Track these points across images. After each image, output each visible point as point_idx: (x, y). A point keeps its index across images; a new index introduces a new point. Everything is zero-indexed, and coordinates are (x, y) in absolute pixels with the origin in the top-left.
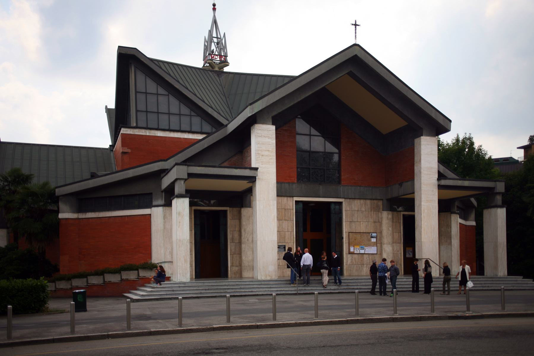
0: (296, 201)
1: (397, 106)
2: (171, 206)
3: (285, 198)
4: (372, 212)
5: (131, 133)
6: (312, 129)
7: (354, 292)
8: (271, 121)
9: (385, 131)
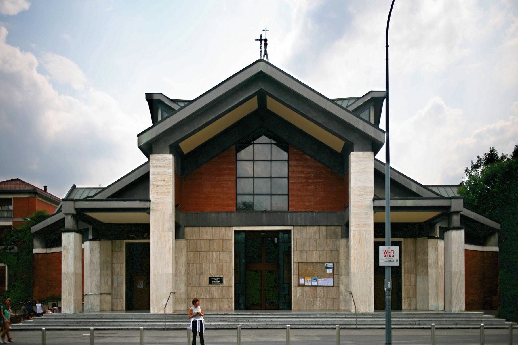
0: (235, 231)
3: (224, 228)
4: (328, 240)
7: (139, 329)
8: (168, 150)
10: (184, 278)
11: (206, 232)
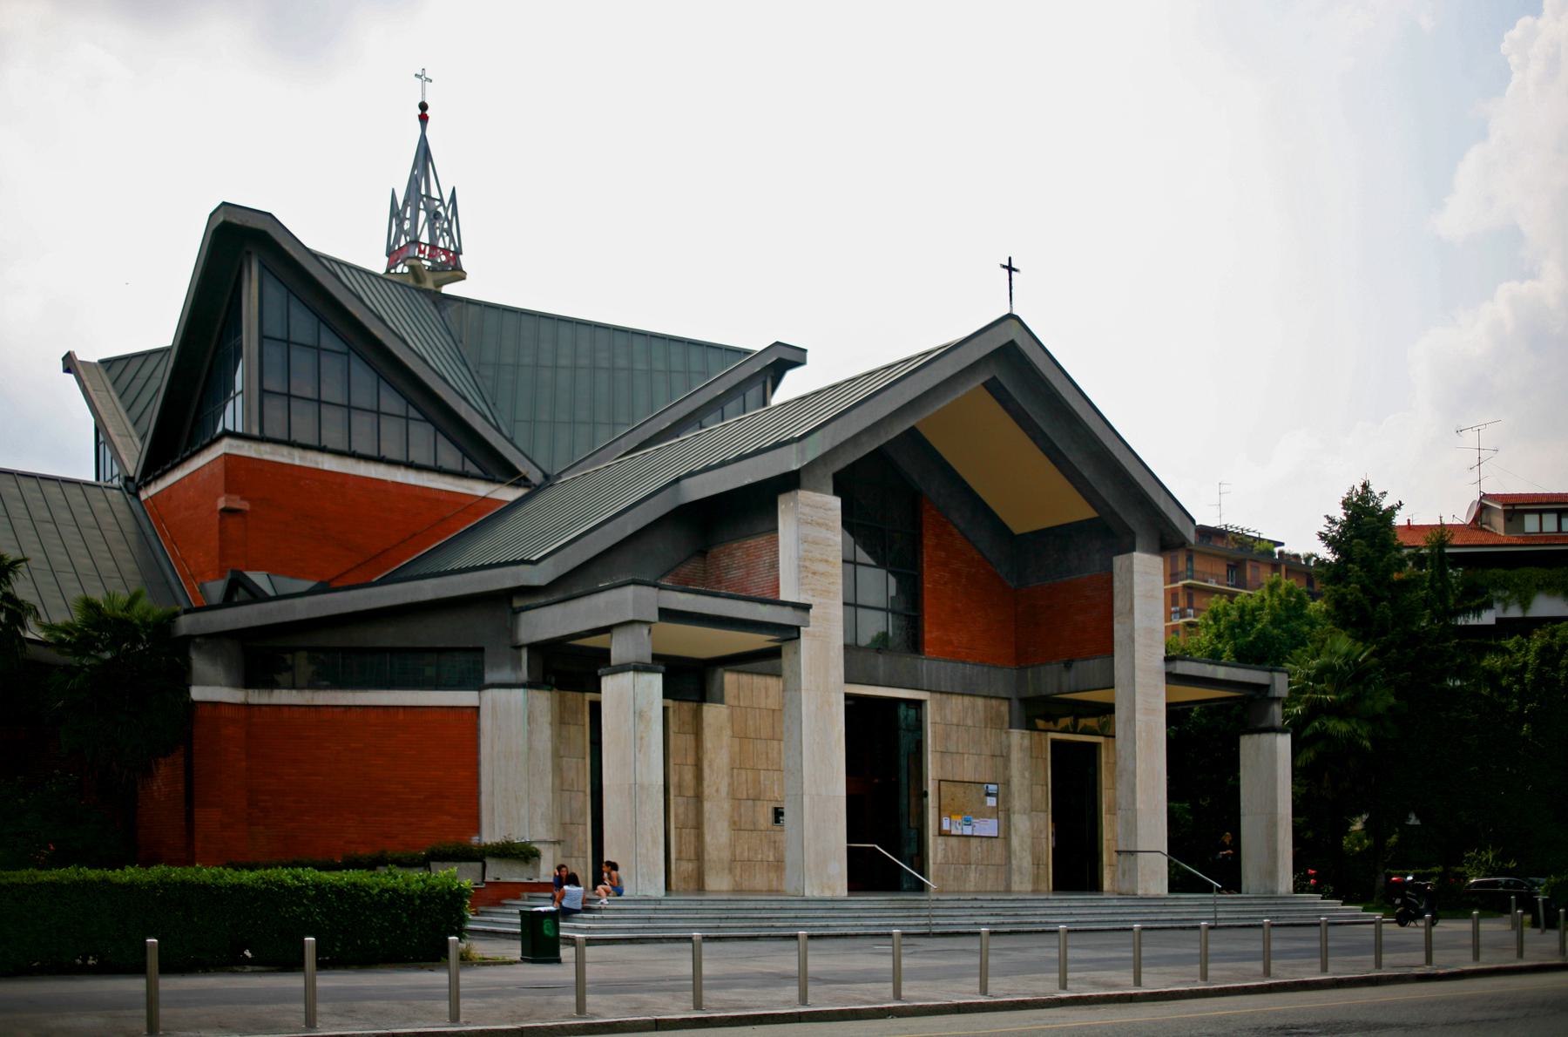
1: (1086, 474)
2: (1168, 705)
5: (253, 454)
6: (467, 461)
7: (978, 934)
9: (1018, 526)
10: (726, 806)
11: (767, 689)
